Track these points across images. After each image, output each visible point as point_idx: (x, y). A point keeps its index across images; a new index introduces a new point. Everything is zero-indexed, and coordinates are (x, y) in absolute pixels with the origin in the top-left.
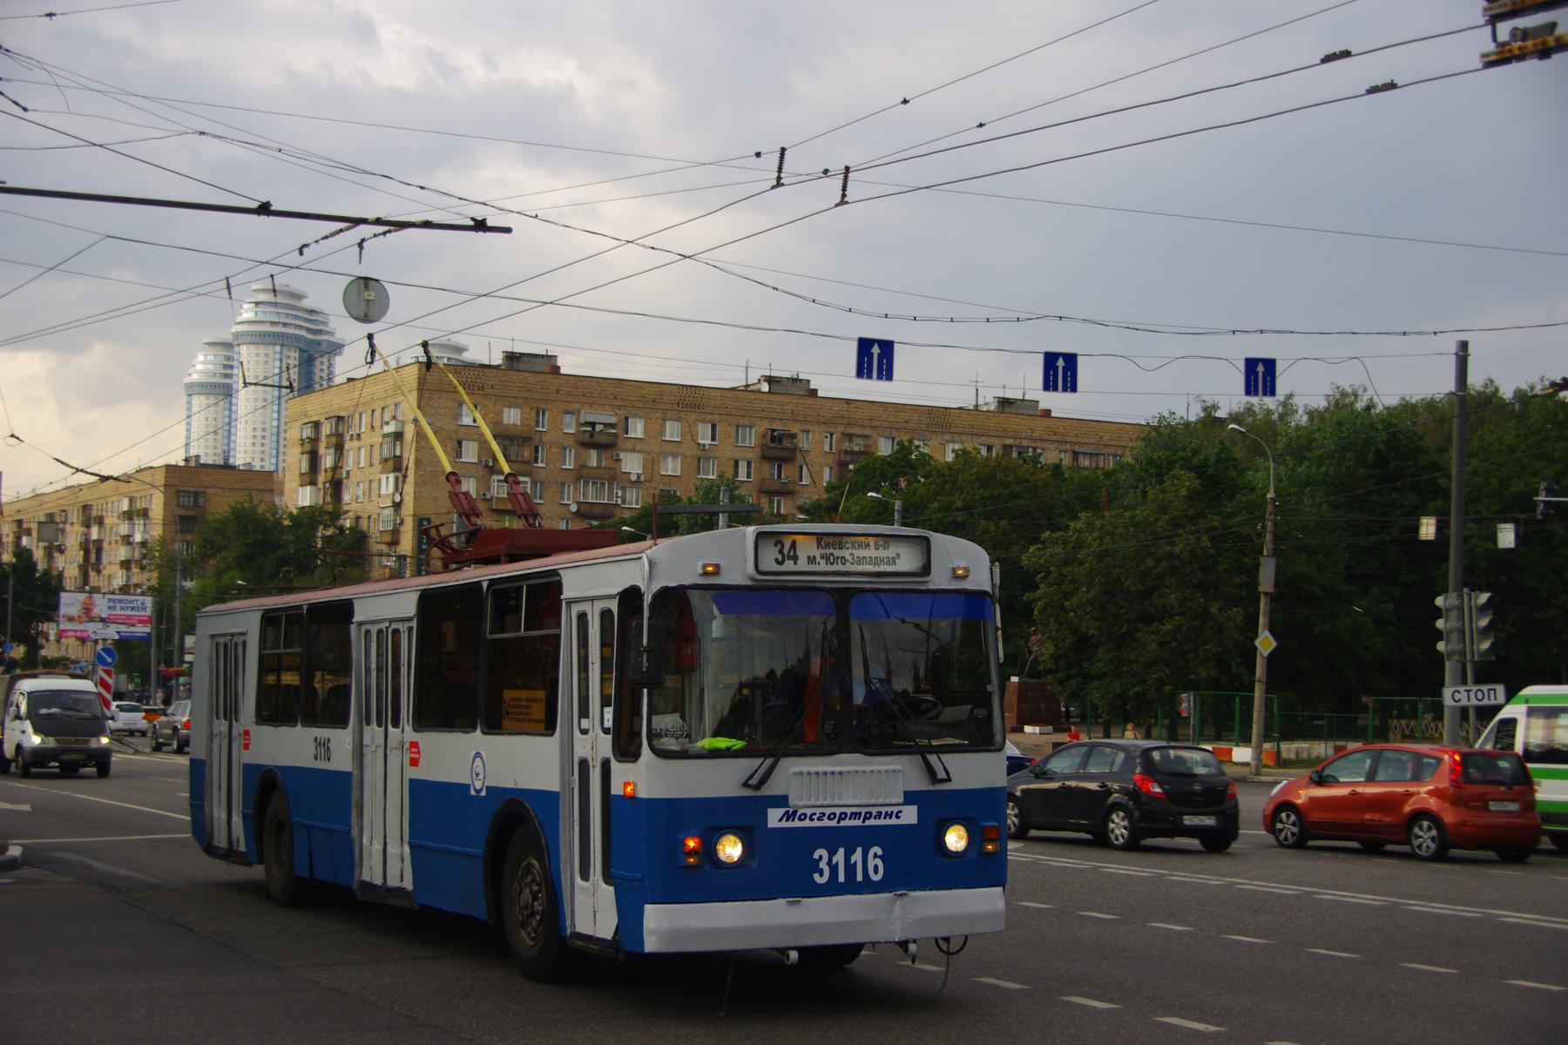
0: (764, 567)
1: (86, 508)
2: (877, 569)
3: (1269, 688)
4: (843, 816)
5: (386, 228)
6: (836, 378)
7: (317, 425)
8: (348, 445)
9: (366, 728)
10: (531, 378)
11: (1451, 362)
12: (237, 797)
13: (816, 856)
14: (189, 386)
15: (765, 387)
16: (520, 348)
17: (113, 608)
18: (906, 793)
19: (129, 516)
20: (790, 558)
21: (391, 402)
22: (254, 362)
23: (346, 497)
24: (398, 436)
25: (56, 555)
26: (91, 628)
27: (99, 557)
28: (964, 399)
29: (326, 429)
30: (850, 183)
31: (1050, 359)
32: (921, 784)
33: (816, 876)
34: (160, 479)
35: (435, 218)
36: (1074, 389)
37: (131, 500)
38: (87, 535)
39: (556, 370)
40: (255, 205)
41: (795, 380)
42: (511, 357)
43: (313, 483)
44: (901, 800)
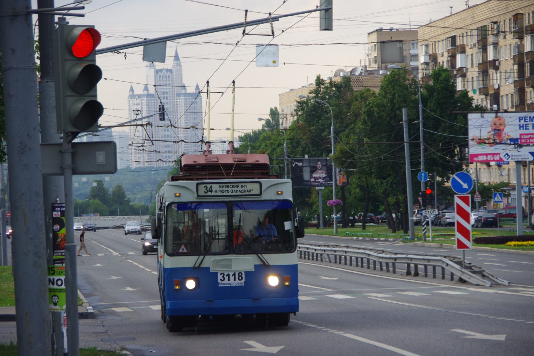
0: (200, 194)
2: (242, 194)
17: (525, 127)
20: (209, 191)
25: (491, 71)
26: (499, 149)
30: (232, 105)
38: (520, 47)
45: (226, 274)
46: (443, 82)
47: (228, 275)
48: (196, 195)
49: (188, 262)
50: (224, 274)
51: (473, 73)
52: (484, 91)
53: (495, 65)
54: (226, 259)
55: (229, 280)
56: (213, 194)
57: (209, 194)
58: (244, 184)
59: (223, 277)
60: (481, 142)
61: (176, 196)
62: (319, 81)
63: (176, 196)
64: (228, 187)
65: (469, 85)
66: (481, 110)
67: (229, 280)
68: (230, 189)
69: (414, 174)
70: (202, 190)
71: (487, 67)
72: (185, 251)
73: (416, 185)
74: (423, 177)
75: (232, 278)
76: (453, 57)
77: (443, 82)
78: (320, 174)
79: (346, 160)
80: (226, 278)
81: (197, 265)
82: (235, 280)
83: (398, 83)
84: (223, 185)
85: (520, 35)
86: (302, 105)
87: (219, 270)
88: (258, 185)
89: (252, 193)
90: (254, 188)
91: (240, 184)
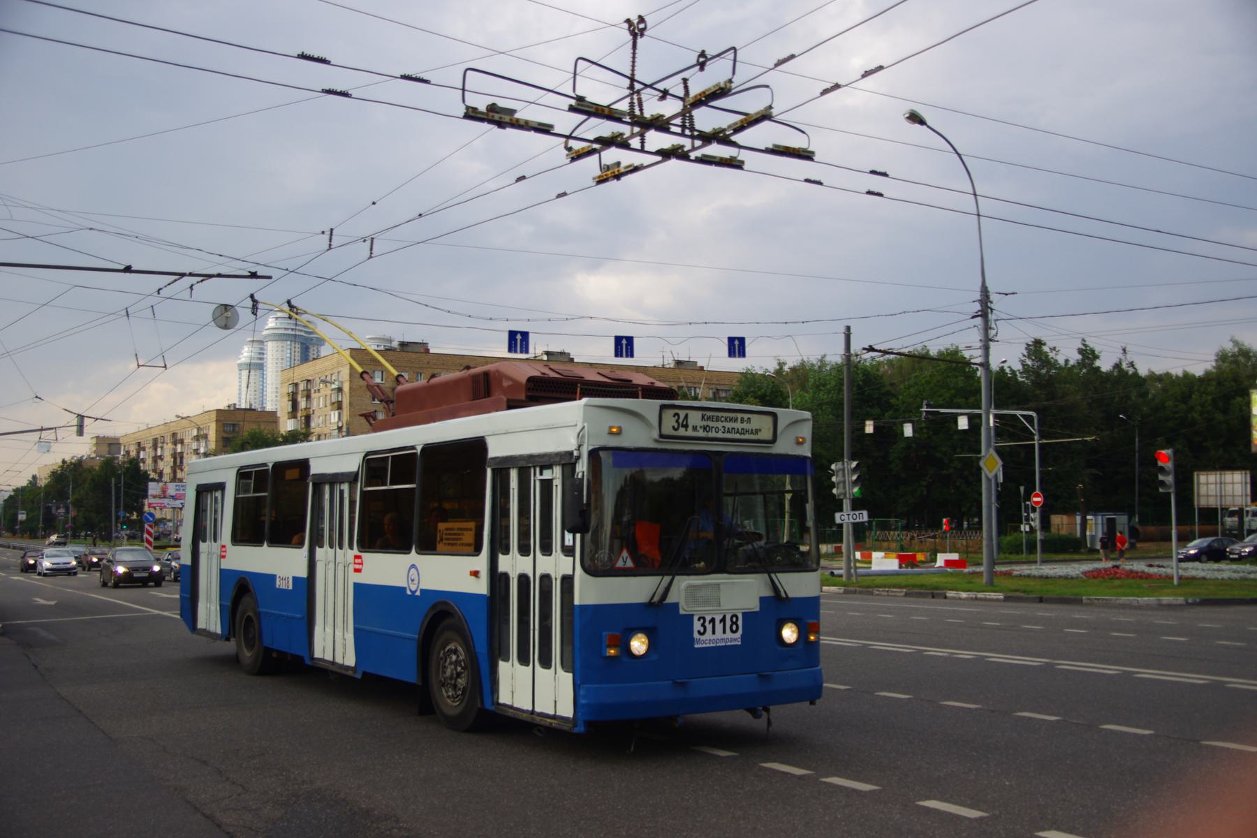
1: (174, 435)
2: (742, 437)
3: (791, 517)
5: (200, 279)
6: (717, 360)
7: (296, 385)
8: (313, 395)
9: (318, 550)
10: (414, 356)
11: (842, 338)
14: (240, 365)
15: (545, 358)
16: (407, 340)
19: (197, 438)
21: (335, 371)
22: (272, 349)
23: (313, 425)
24: (340, 390)
26: (166, 501)
27: (181, 462)
28: (658, 362)
29: (301, 387)
31: (618, 340)
34: (214, 416)
35: (223, 272)
36: (744, 356)
37: (199, 429)
38: (175, 450)
39: (427, 351)
40: (122, 267)
41: (562, 353)
42: (679, 363)
43: (295, 417)
45: (708, 618)
46: (135, 463)
47: (713, 621)
48: (656, 434)
49: (634, 590)
50: (704, 619)
51: (149, 461)
52: (155, 471)
53: (161, 458)
54: (708, 585)
55: (714, 633)
56: (690, 433)
57: (682, 432)
58: (746, 416)
59: (703, 625)
60: (154, 497)
61: (611, 433)
62: (64, 462)
63: (611, 433)
64: (718, 419)
65: (147, 466)
66: (153, 480)
67: (714, 633)
68: (719, 425)
69: (117, 512)
70: (669, 420)
71: (156, 459)
72: (630, 564)
73: (118, 517)
74: (121, 513)
75: (719, 627)
76: (138, 453)
77: (135, 463)
78: (62, 511)
79: (77, 504)
80: (709, 627)
81: (656, 599)
82: (724, 632)
83: (109, 464)
84: (709, 414)
85: (175, 443)
86: (54, 473)
87: (697, 610)
88: (768, 421)
89: (760, 436)
90: (762, 426)
91: (739, 416)
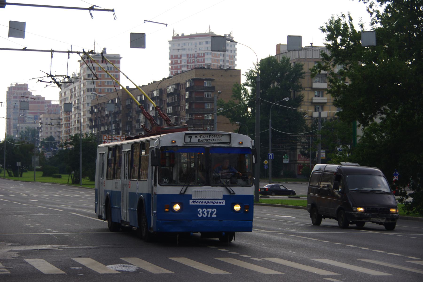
4: (208, 202)
12: (103, 197)
13: (198, 210)
18: (224, 195)
32: (226, 193)
33: (198, 215)
40: (22, 48)
44: (222, 198)
